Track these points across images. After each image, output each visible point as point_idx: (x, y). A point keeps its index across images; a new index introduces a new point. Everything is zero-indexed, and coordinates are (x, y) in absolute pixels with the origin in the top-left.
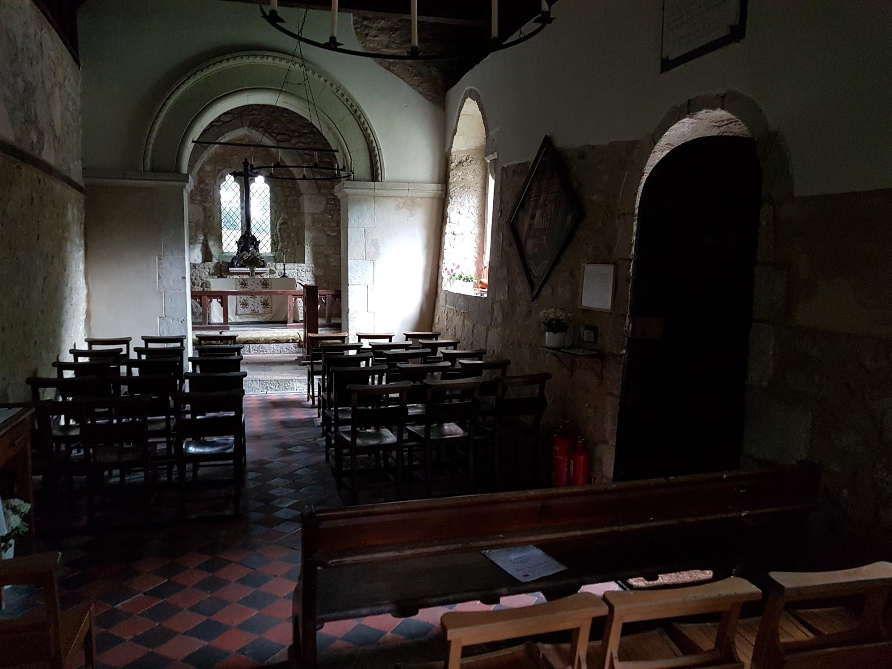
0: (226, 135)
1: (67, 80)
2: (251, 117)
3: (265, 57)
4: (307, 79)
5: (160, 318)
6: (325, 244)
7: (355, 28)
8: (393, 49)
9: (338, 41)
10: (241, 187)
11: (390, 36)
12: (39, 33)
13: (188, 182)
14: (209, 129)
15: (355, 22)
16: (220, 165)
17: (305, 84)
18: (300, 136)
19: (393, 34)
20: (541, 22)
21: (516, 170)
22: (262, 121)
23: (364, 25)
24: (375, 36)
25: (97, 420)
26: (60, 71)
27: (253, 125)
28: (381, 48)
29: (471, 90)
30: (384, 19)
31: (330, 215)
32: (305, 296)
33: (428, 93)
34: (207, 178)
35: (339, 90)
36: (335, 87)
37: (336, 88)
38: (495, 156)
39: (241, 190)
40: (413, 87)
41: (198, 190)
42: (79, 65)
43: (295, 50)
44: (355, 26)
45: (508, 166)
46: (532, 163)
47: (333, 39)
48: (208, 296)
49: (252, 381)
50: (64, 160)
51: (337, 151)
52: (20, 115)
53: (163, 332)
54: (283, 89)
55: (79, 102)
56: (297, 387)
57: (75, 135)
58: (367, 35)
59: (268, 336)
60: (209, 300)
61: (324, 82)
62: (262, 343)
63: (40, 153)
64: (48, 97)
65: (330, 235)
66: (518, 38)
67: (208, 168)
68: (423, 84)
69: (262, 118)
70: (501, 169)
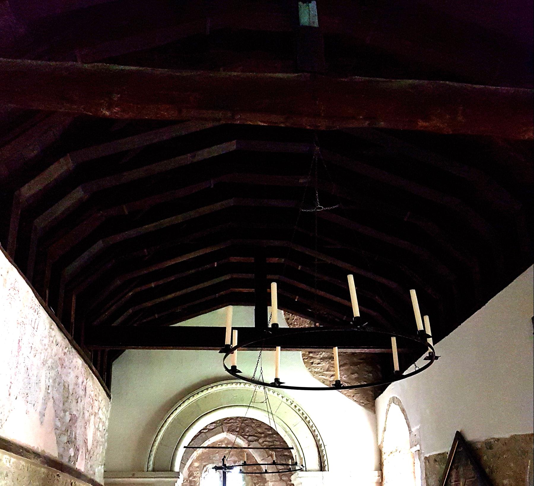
0: (210, 439)
1: (100, 410)
2: (229, 425)
4: (268, 398)
7: (303, 359)
9: (281, 381)
12: (85, 381)
13: (179, 478)
14: (198, 435)
16: (204, 462)
17: (266, 402)
18: (265, 437)
20: (429, 360)
21: (439, 458)
23: (309, 356)
24: (318, 364)
26: (96, 403)
27: (231, 430)
29: (393, 398)
33: (361, 401)
34: (195, 472)
35: (292, 403)
36: (289, 401)
38: (418, 448)
40: (349, 397)
41: (188, 481)
42: (110, 398)
43: (259, 379)
44: (304, 358)
45: (430, 456)
46: (449, 453)
47: (277, 380)
50: (91, 467)
51: (292, 448)
52: (65, 439)
54: (250, 405)
55: (107, 424)
57: (101, 447)
58: (312, 363)
63: (74, 464)
64: (86, 423)
66: (415, 370)
67: (196, 464)
68: (357, 395)
69: (237, 425)
70: (424, 459)
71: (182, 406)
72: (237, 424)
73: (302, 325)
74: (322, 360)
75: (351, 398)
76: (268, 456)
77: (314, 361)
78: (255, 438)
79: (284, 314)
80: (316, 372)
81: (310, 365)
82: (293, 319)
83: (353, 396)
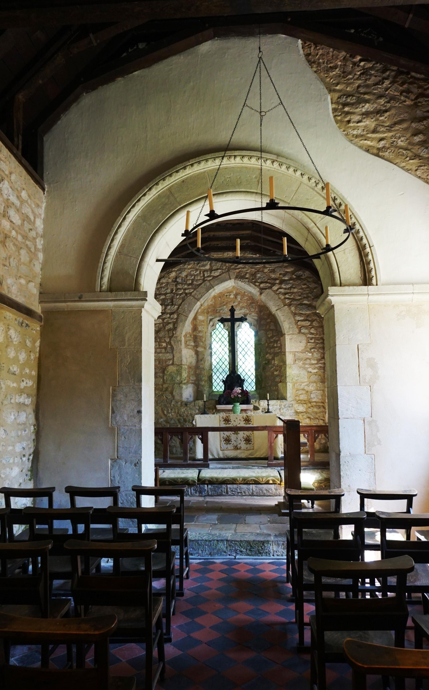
0: (215, 287)
2: (237, 271)
3: (233, 158)
5: (111, 459)
6: (306, 381)
7: (335, 116)
8: (383, 132)
10: (229, 332)
11: (377, 120)
13: (146, 300)
15: (334, 110)
16: (211, 315)
18: (281, 283)
19: (381, 116)
22: (247, 273)
23: (345, 112)
25: (81, 558)
28: (367, 134)
30: (369, 103)
31: (310, 353)
32: (286, 432)
35: (318, 183)
37: (315, 181)
39: (229, 335)
40: (410, 172)
41: (192, 336)
42: (43, 189)
44: (336, 114)
48: (169, 433)
49: (218, 541)
53: (114, 477)
56: (274, 551)
58: (349, 122)
59: (247, 475)
60: (275, 435)
61: (301, 176)
62: (240, 484)
65: (311, 372)
68: (422, 168)
71: (147, 196)
72: (246, 269)
73: (332, 63)
74: (364, 116)
75: (413, 173)
76: (284, 306)
77: (352, 117)
78: (267, 285)
79: (303, 48)
80: (355, 136)
81: (345, 126)
82: (317, 55)
83: (416, 170)
